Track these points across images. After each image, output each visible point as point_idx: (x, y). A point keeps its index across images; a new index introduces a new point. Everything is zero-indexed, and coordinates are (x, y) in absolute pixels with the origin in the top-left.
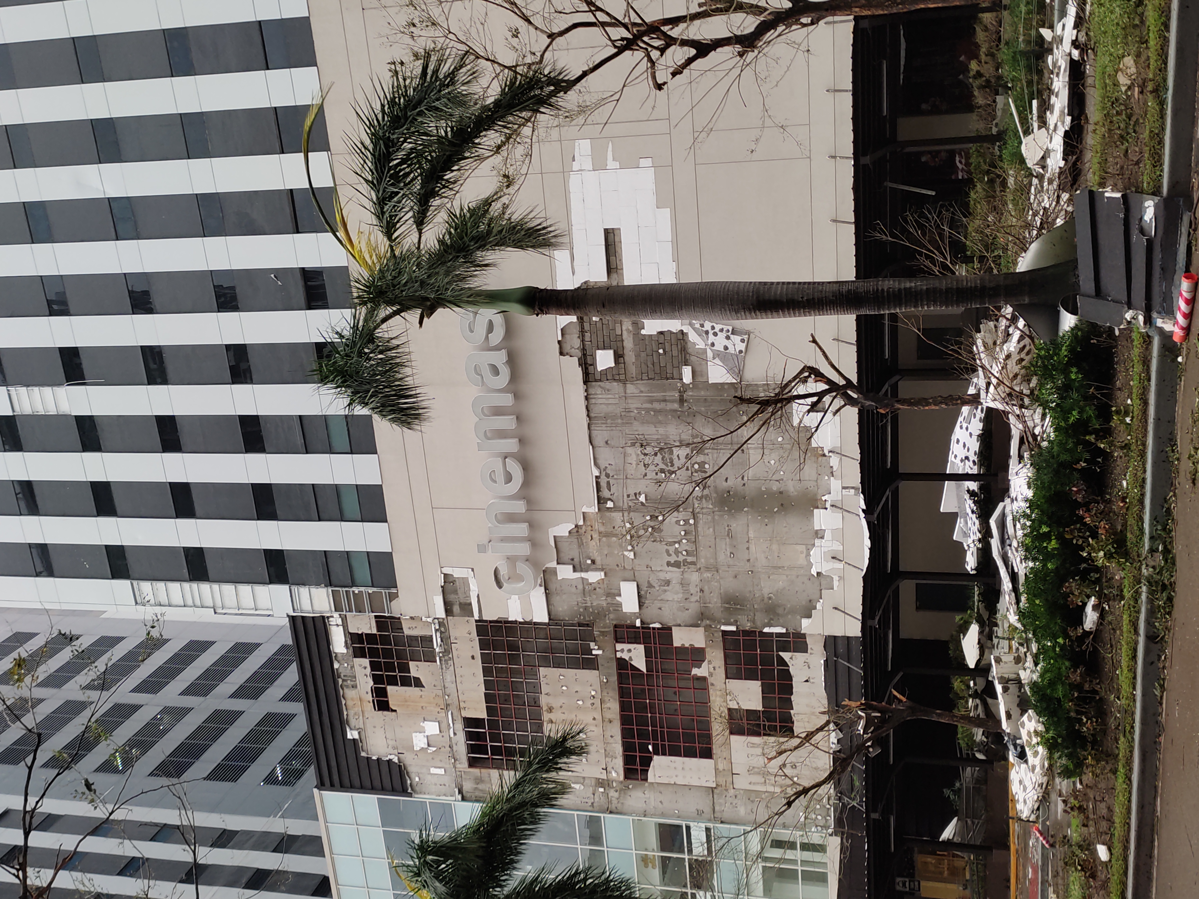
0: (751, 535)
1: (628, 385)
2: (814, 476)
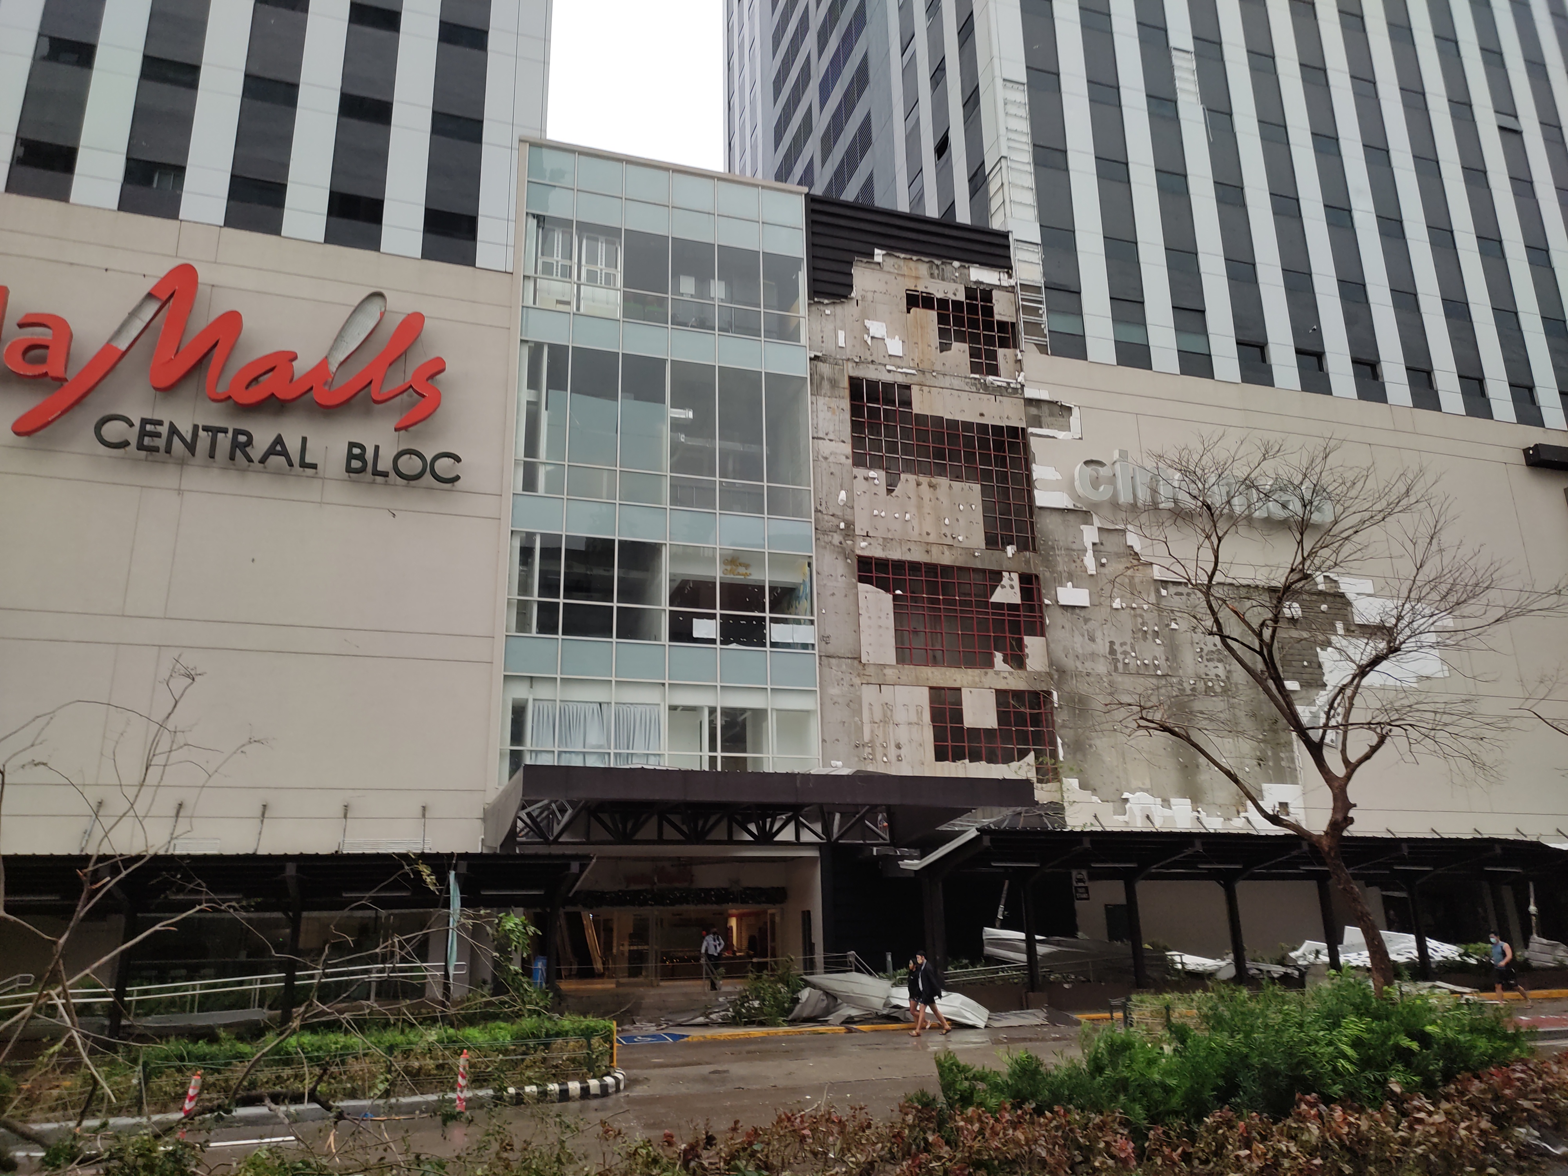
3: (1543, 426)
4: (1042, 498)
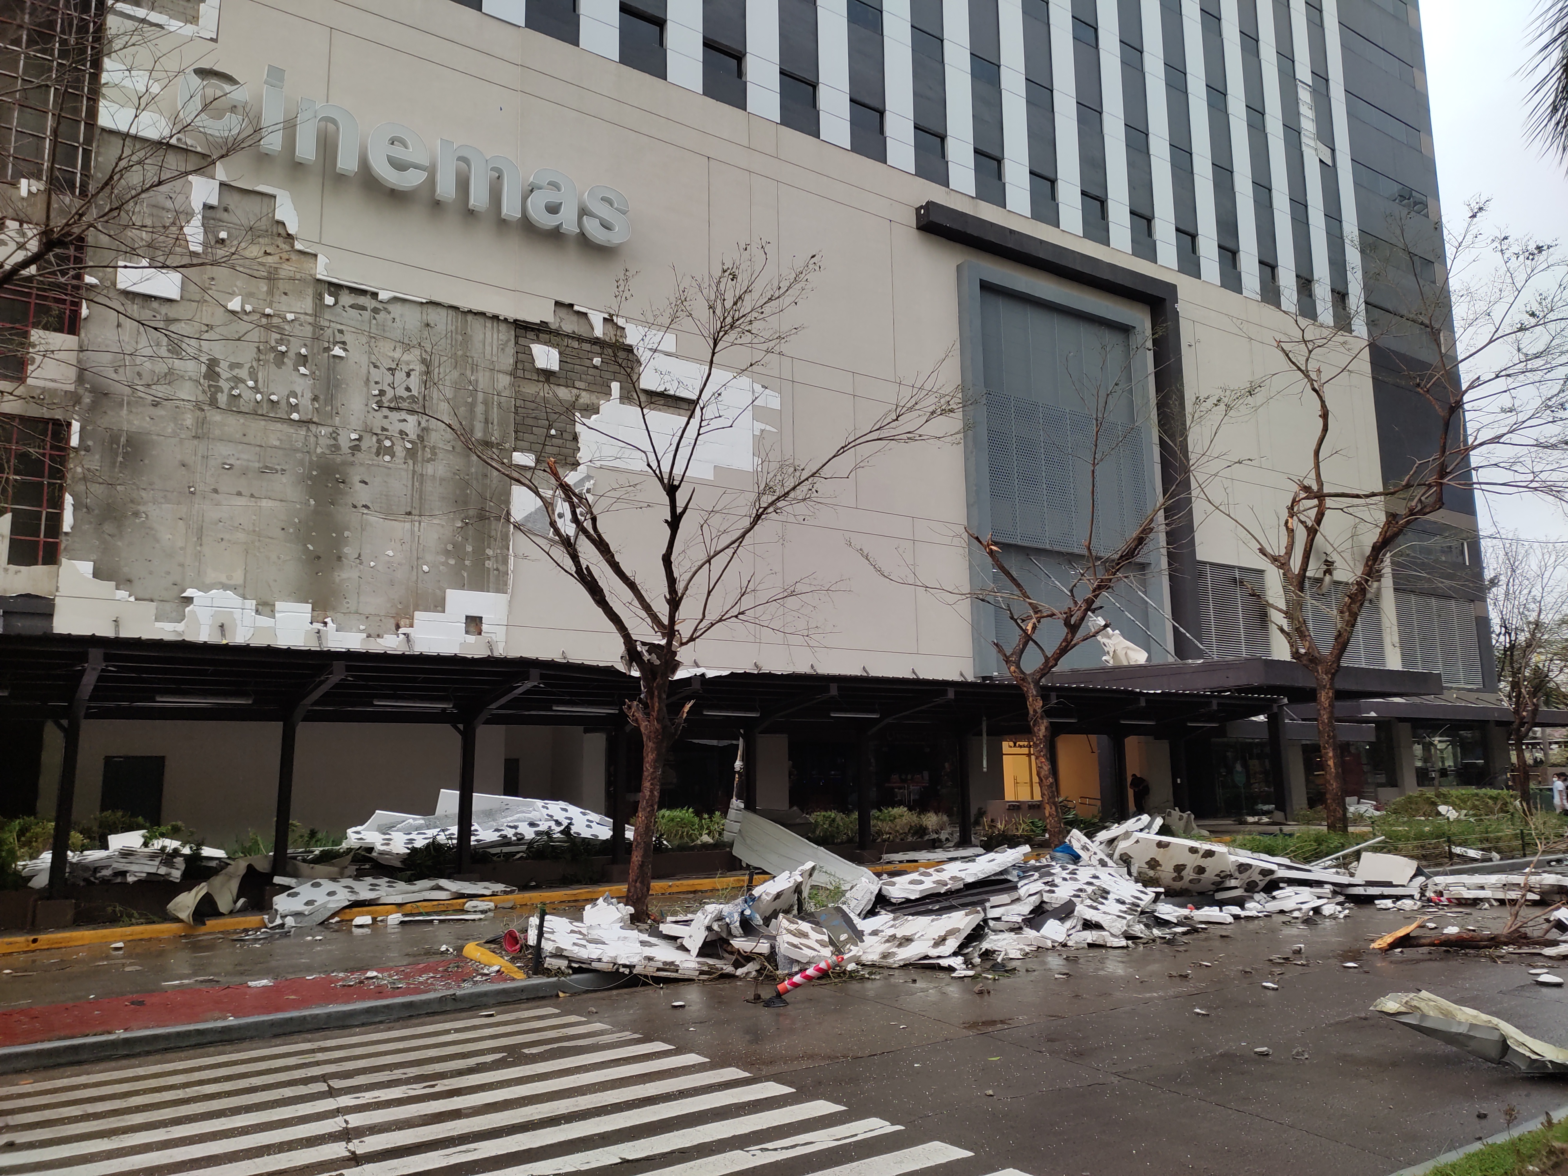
0: (264, 503)
1: (508, 377)
3: (948, 186)
4: (111, 115)
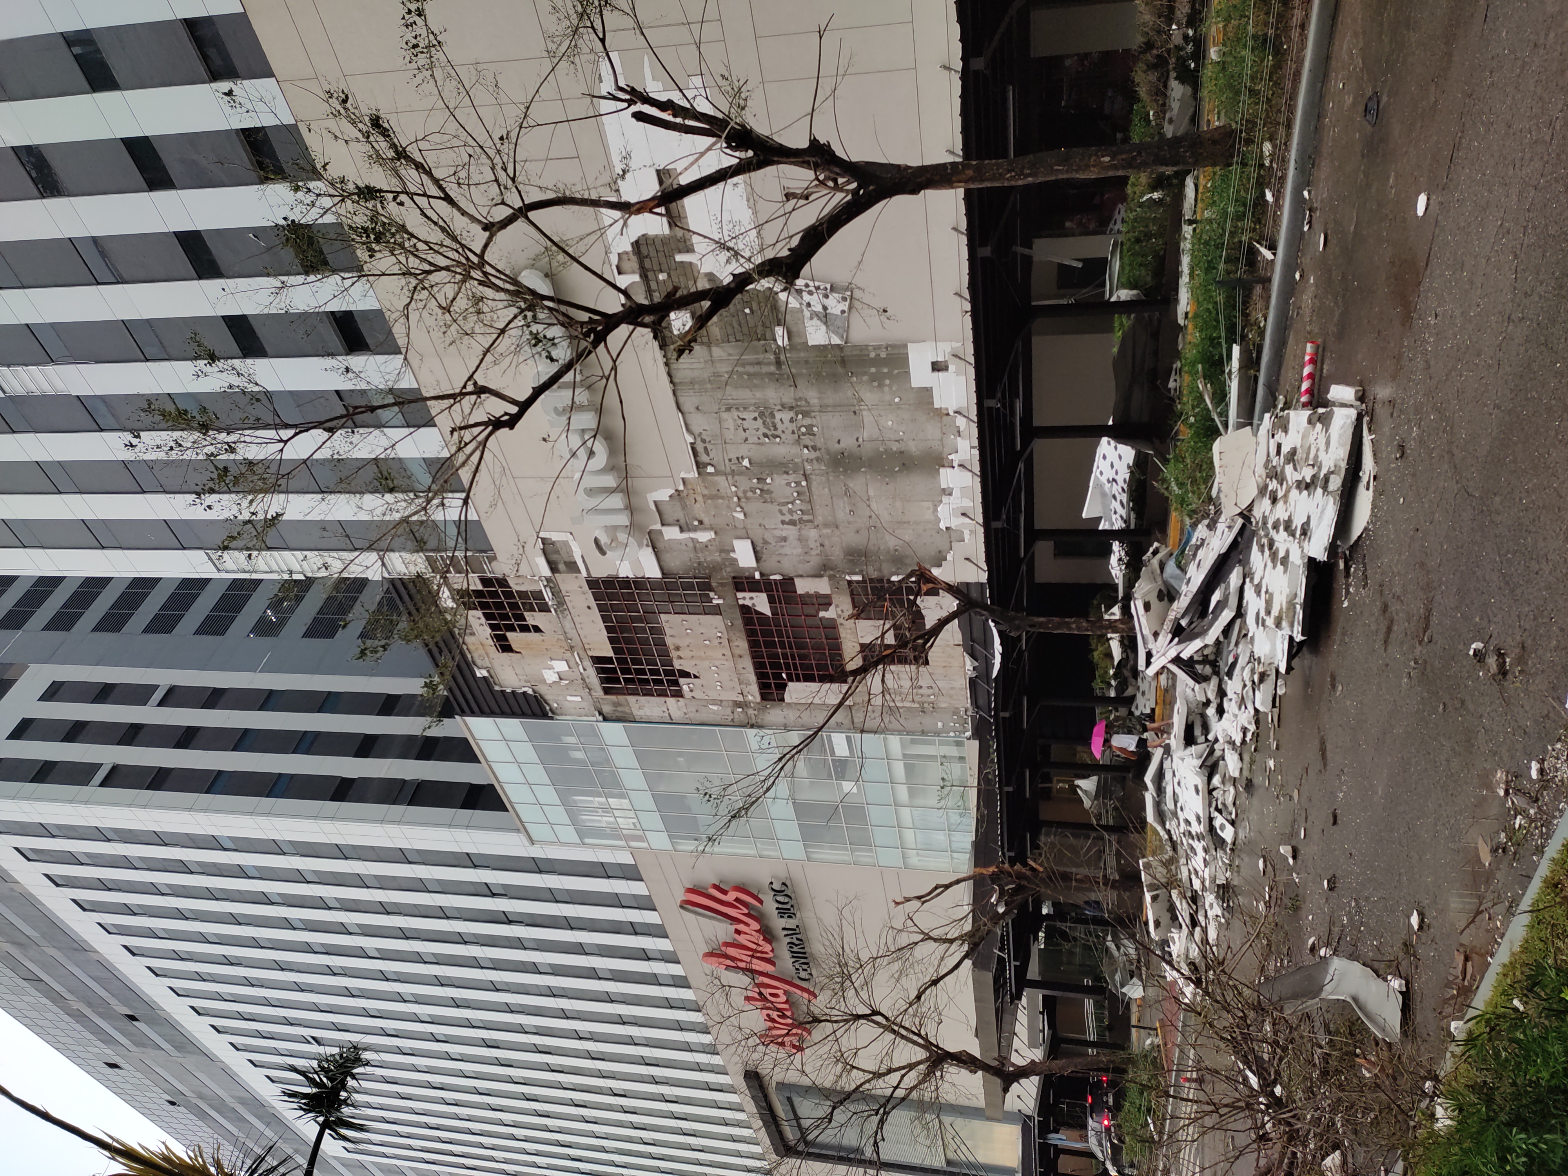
2: (938, 434)
